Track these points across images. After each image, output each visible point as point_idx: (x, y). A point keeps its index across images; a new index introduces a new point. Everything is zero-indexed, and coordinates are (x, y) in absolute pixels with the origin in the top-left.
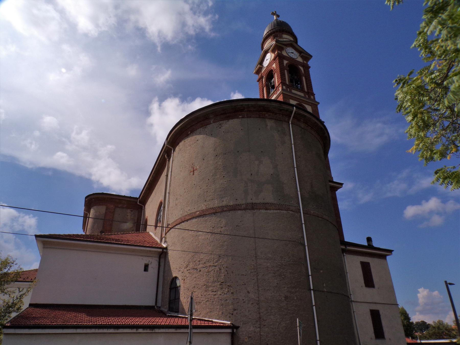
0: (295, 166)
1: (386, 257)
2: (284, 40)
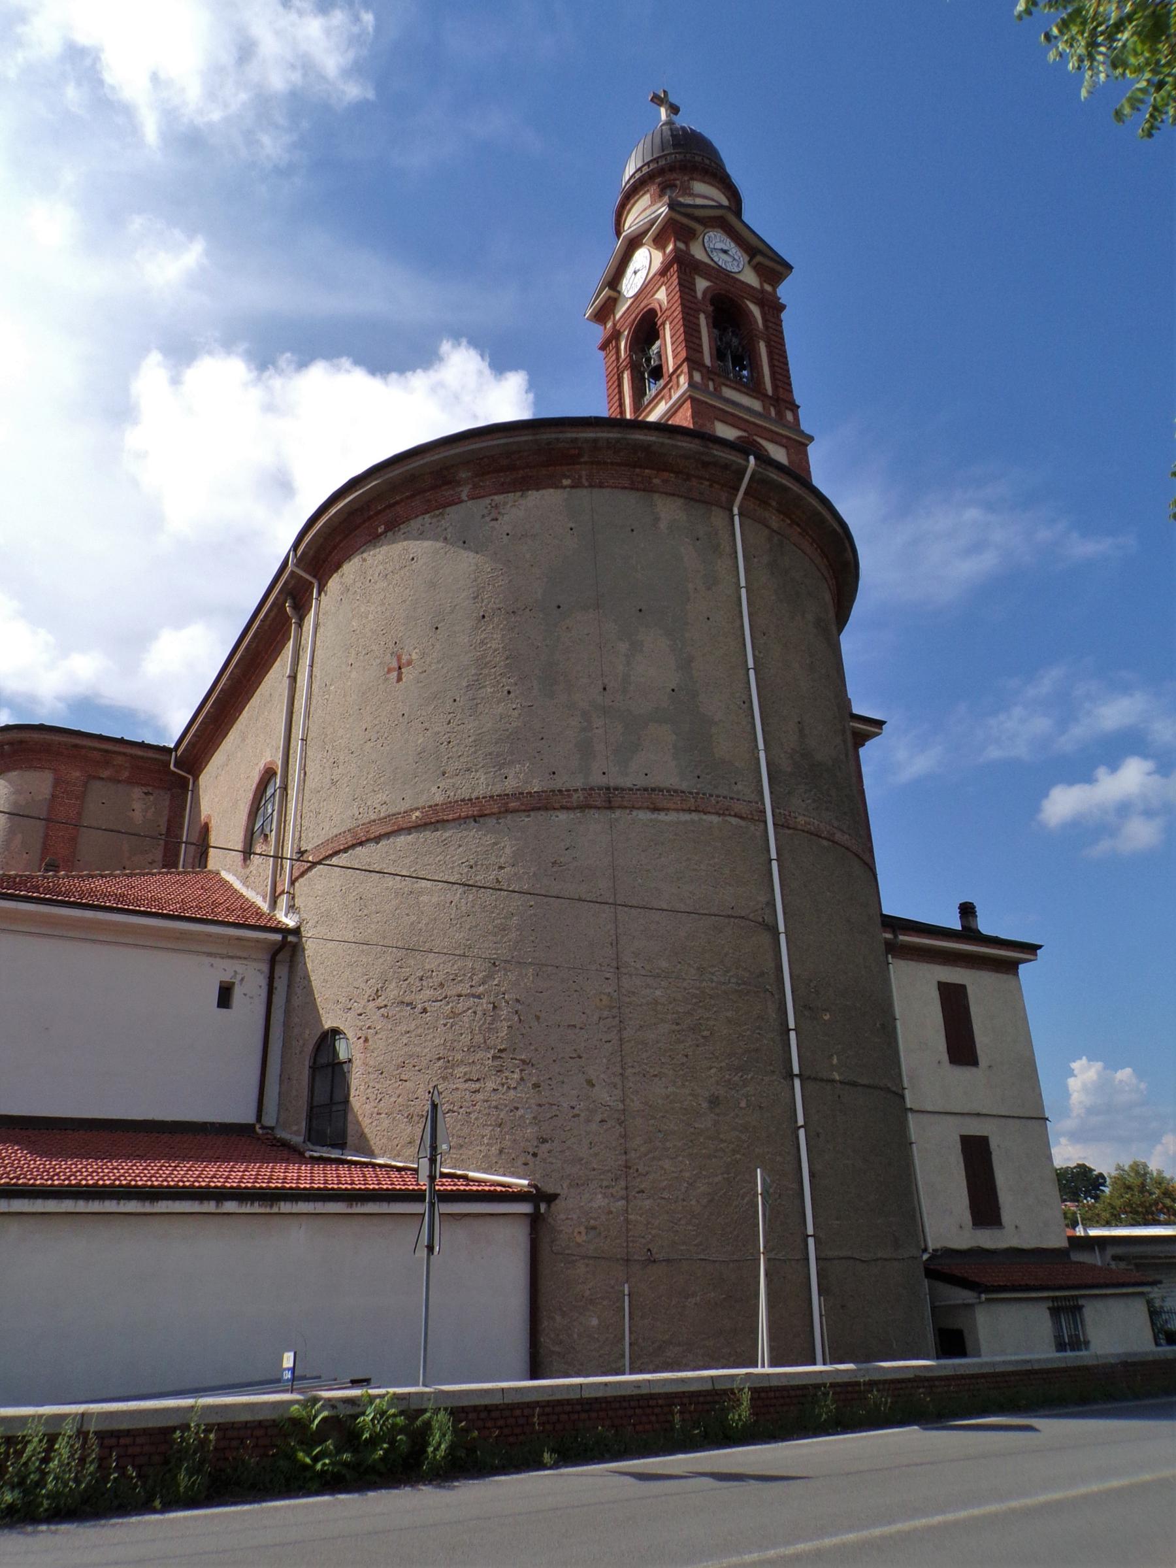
0: (751, 664)
1: (1018, 968)
2: (699, 201)
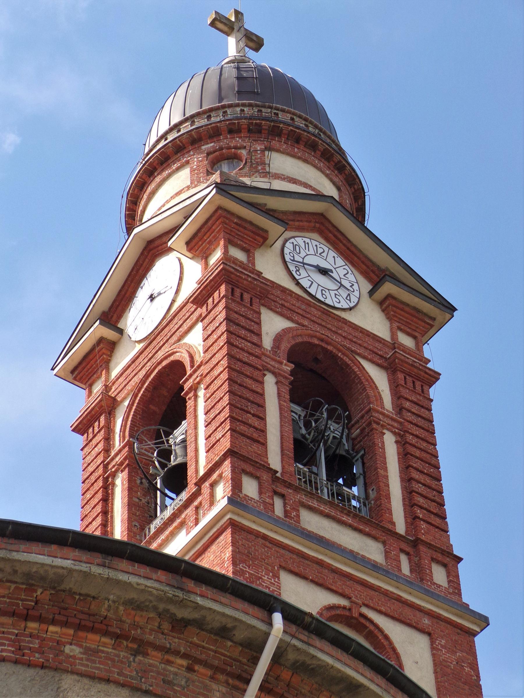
2: (278, 185)
